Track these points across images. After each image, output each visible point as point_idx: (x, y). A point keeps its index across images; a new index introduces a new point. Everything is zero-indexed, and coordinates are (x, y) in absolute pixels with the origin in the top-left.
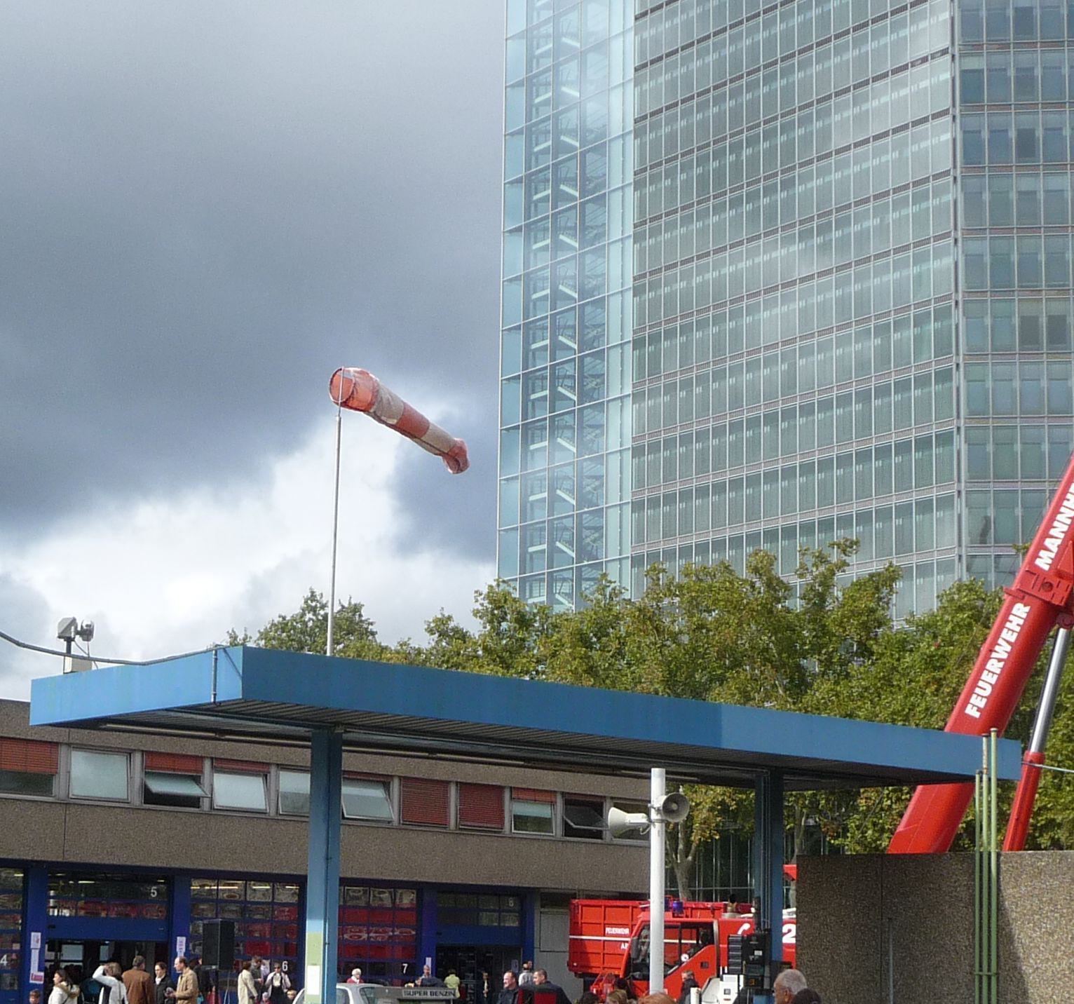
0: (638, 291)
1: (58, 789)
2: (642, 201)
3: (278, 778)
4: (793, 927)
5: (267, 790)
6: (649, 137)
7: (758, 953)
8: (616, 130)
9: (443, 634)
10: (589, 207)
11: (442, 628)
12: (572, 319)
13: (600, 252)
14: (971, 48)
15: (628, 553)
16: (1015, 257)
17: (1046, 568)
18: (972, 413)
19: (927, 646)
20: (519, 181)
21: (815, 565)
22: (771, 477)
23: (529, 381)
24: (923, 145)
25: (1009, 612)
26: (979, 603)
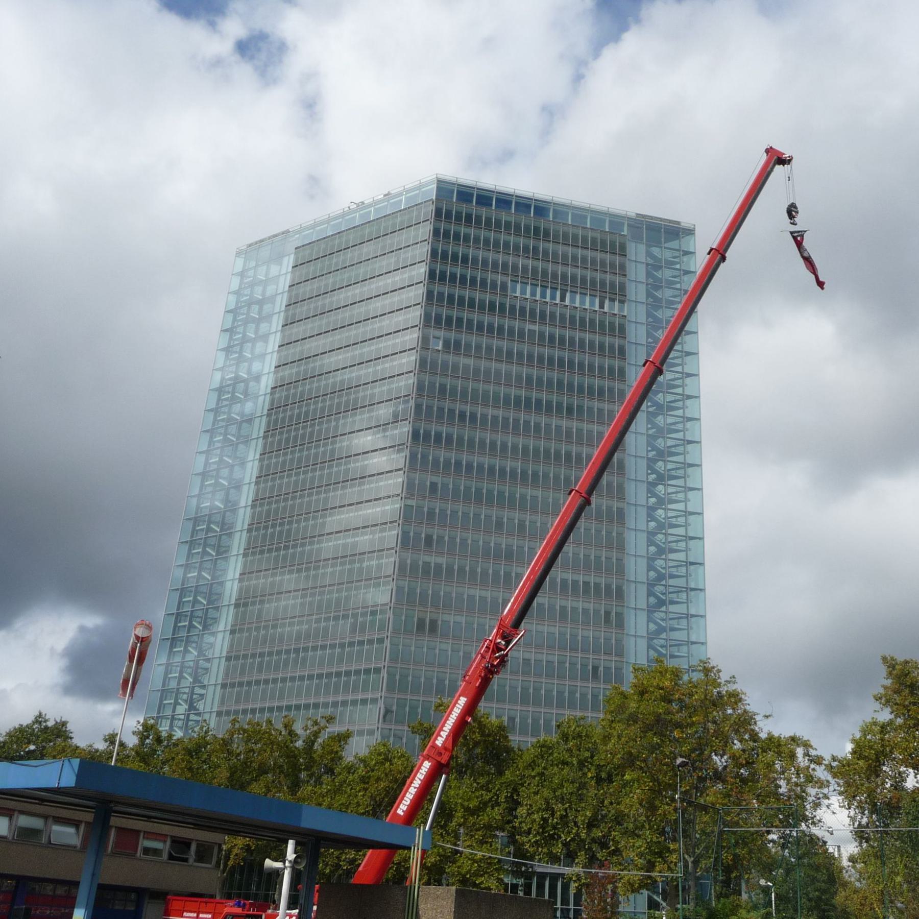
2: (250, 538)
3: (18, 818)
5: (10, 824)
6: (258, 509)
12: (204, 589)
16: (418, 591)
17: (440, 745)
18: (391, 660)
19: (361, 771)
21: (313, 725)
22: (293, 679)
23: (178, 616)
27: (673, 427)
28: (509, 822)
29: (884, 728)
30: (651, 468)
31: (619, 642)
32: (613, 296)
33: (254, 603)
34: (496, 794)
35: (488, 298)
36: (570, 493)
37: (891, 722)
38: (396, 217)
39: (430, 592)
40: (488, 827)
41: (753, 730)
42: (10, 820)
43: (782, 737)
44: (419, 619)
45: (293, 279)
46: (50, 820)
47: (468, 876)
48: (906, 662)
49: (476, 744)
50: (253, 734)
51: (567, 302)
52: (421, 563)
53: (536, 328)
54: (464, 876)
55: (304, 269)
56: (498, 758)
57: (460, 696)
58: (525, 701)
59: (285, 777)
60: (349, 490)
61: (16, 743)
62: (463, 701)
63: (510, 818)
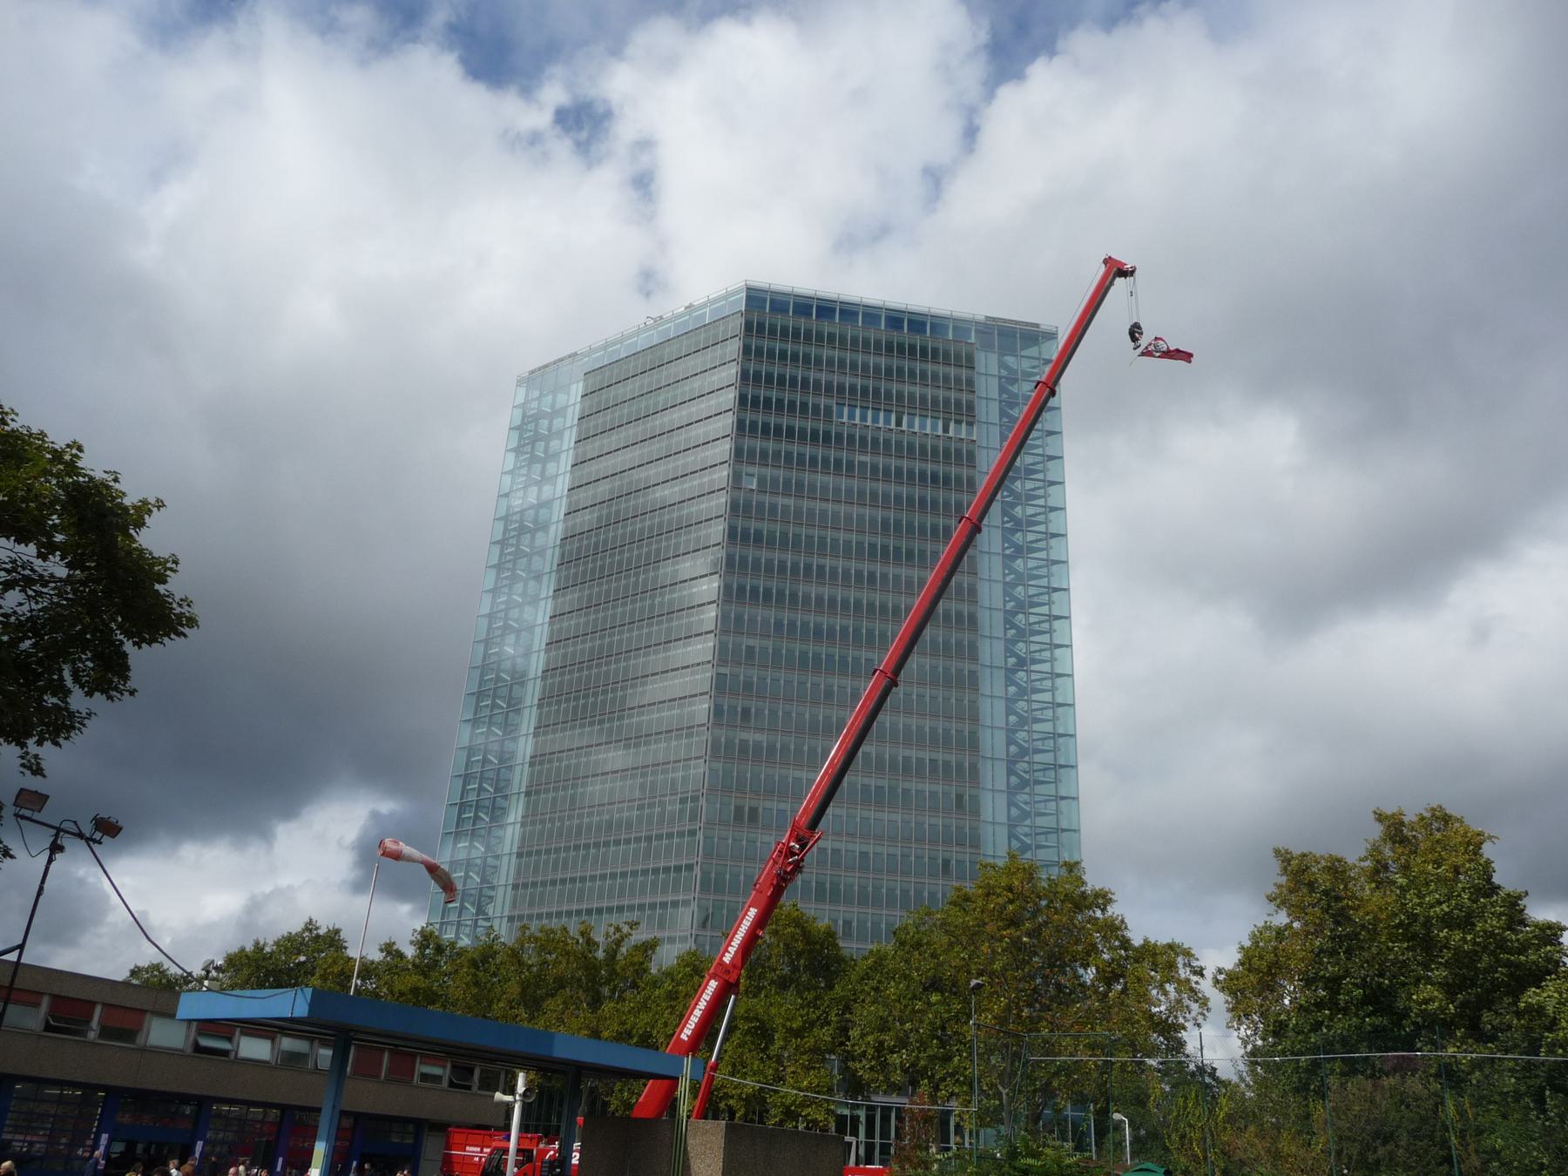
0: (532, 764)
1: (140, 1040)
2: (541, 714)
4: (578, 1155)
5: (273, 1048)
7: (558, 1170)
8: (532, 675)
9: (389, 953)
10: (511, 714)
11: (389, 949)
12: (491, 775)
13: (515, 739)
14: (725, 631)
15: (506, 914)
18: (705, 855)
19: (668, 986)
20: (473, 694)
23: (463, 807)
24: (693, 708)
25: (707, 984)
26: (697, 963)
27: (1035, 572)
28: (842, 1044)
29: (1280, 933)
30: (1009, 623)
31: (974, 830)
32: (959, 417)
33: (547, 791)
34: (824, 1012)
35: (809, 425)
36: (874, 674)
37: (1289, 926)
38: (700, 333)
39: (749, 775)
40: (815, 1050)
41: (1123, 936)
42: (273, 1042)
43: (1159, 944)
44: (736, 807)
45: (583, 410)
46: (317, 1042)
47: (793, 1108)
48: (1304, 855)
49: (800, 955)
50: (549, 942)
51: (904, 427)
52: (737, 741)
53: (867, 459)
54: (788, 1108)
55: (595, 398)
56: (828, 969)
57: (750, 907)
58: (863, 901)
59: (584, 991)
60: (652, 657)
61: (285, 953)
62: (753, 912)
63: (843, 1039)
